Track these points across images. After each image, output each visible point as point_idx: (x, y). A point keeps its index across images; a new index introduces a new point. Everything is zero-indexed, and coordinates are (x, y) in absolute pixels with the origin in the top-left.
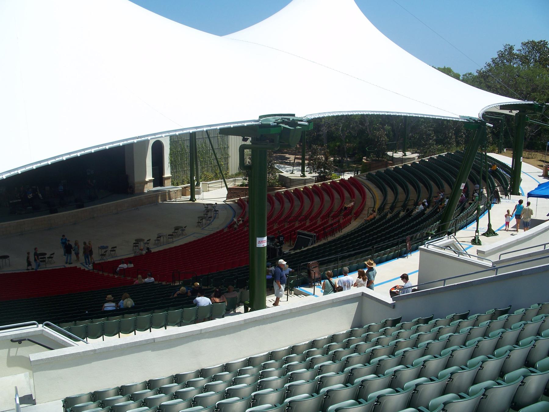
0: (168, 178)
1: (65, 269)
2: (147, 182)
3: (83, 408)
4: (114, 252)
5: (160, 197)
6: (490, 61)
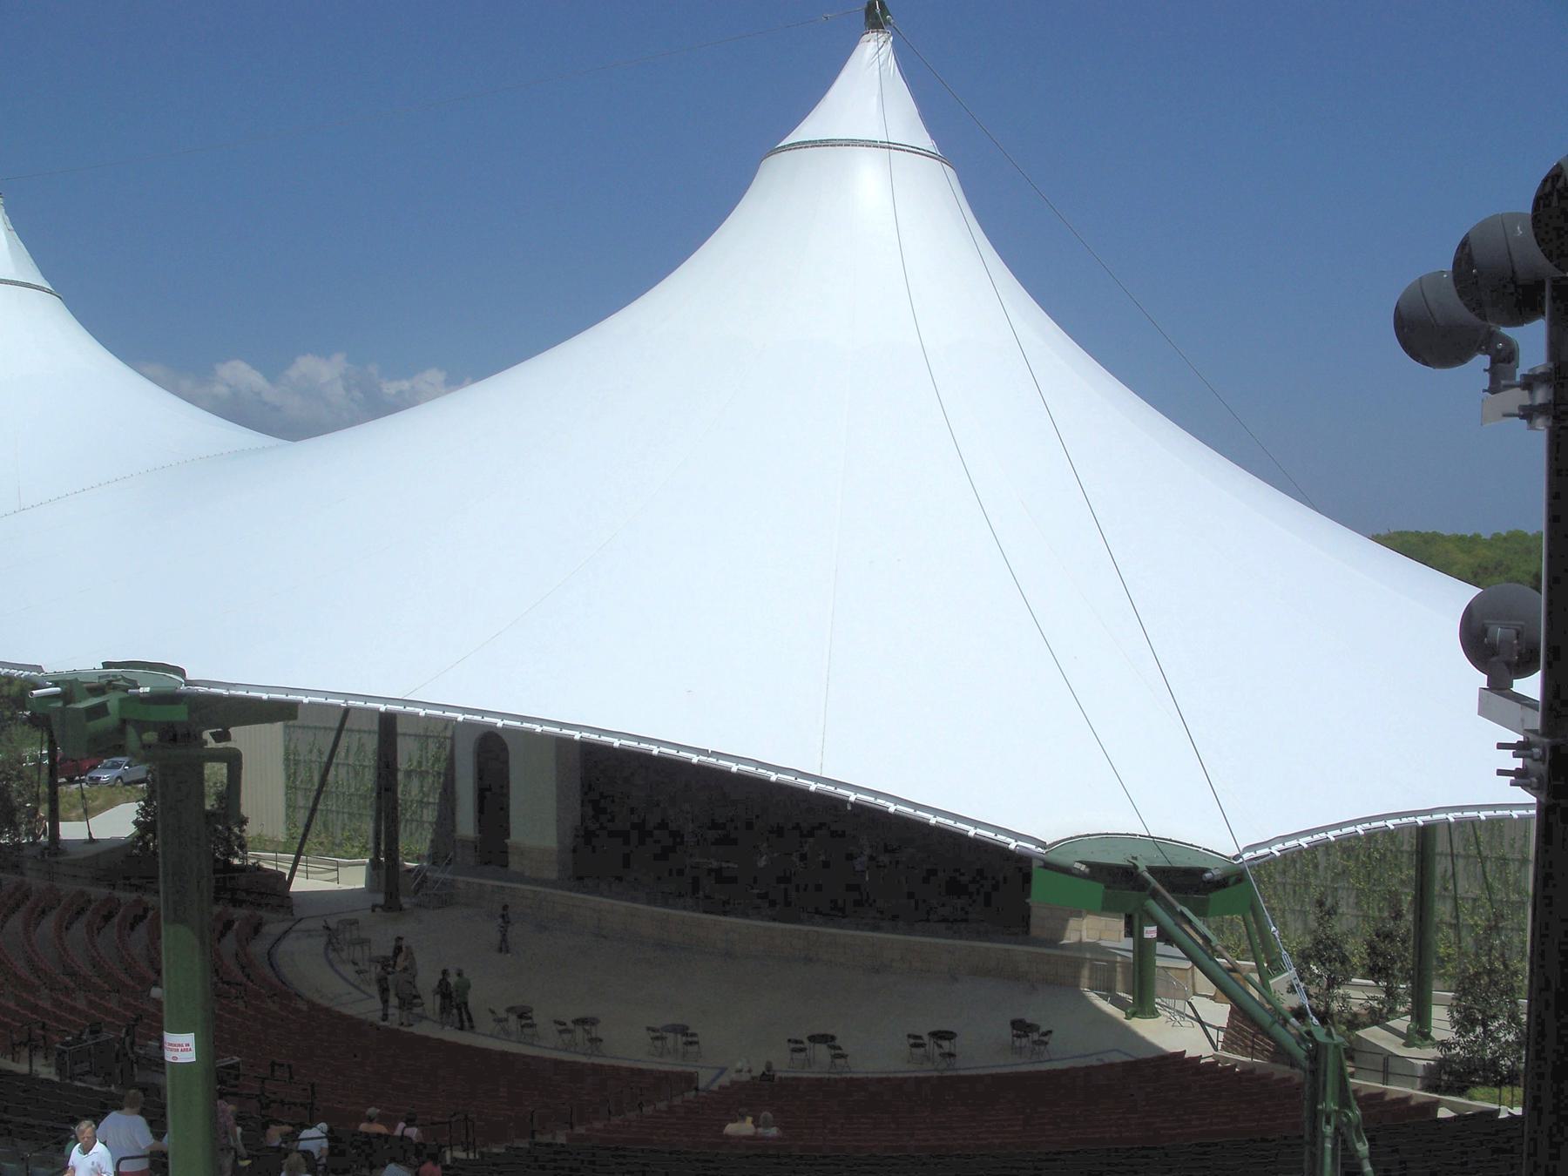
5: (1086, 972)
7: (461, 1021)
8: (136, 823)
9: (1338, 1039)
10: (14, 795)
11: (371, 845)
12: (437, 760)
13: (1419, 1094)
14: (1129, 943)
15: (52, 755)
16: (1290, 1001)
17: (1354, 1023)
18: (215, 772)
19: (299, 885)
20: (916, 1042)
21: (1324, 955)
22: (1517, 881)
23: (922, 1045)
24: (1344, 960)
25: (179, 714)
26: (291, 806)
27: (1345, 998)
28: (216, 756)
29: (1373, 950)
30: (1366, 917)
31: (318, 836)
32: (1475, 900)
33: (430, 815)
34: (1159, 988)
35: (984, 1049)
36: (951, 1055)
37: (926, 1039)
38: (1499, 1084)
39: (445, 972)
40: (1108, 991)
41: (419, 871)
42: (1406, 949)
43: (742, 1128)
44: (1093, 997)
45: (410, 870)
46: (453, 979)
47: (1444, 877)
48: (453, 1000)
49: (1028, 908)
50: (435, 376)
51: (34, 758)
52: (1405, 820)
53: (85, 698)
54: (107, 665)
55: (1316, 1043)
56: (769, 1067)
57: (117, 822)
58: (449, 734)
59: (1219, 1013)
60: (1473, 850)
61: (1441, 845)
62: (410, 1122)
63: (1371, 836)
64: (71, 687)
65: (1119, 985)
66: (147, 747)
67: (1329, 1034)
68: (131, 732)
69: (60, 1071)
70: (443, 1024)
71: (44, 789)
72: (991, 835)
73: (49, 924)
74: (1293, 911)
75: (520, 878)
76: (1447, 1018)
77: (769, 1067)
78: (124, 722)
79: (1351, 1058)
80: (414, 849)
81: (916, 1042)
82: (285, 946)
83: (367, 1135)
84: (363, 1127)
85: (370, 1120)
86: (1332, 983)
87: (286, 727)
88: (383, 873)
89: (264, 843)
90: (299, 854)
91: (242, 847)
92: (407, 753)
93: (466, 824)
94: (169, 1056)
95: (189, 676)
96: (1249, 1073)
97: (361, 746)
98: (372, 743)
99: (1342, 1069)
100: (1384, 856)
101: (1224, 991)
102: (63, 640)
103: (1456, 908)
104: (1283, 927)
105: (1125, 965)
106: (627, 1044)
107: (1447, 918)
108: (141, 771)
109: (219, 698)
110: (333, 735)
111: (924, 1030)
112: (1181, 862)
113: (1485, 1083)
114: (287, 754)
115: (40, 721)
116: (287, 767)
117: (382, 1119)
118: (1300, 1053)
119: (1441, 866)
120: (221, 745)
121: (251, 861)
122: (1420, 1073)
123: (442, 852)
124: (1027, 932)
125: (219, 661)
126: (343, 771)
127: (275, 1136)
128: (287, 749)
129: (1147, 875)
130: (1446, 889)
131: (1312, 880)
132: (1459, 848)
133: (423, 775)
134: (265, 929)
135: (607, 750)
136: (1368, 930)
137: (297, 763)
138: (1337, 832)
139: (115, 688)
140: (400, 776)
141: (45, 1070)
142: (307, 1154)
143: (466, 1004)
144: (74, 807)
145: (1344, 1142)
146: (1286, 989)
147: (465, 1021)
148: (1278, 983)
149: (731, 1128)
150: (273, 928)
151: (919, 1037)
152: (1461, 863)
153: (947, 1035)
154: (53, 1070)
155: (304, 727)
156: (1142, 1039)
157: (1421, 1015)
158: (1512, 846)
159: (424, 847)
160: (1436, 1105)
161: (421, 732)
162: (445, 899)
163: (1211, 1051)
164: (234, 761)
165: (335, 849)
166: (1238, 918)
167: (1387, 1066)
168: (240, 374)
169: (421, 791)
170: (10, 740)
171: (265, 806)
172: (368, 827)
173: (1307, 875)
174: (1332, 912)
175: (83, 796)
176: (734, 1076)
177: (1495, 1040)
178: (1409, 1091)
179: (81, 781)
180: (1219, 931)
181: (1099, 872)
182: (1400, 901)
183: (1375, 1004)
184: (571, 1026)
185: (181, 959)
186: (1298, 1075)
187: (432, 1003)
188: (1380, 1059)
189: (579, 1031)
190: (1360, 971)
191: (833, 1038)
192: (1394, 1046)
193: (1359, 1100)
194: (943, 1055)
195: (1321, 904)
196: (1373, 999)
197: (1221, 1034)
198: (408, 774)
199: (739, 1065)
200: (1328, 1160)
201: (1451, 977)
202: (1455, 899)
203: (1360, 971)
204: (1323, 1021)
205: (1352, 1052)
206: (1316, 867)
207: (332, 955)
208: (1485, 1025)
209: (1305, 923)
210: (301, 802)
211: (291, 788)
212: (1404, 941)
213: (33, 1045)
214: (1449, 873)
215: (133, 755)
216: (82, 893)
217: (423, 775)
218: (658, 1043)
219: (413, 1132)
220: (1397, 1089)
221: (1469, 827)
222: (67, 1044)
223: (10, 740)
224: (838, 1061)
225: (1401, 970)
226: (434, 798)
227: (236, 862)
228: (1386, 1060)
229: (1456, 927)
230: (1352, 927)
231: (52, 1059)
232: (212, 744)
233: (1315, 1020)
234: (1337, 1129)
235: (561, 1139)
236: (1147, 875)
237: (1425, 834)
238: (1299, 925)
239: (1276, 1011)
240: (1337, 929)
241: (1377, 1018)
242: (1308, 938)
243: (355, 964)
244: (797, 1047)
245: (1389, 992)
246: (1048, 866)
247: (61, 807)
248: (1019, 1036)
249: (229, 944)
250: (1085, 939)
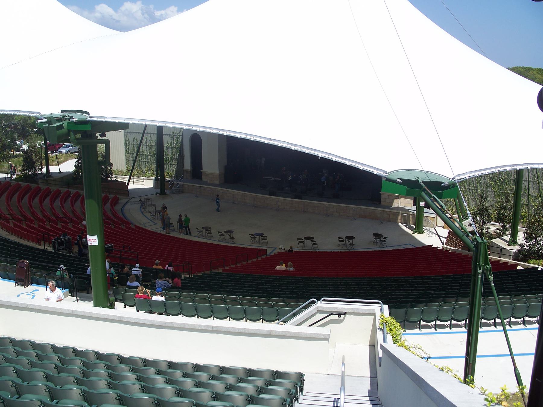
5: (400, 218)
7: (187, 232)
8: (75, 166)
9: (485, 241)
10: (34, 157)
11: (155, 173)
12: (177, 143)
13: (511, 261)
14: (415, 208)
15: (46, 143)
16: (470, 229)
17: (491, 237)
18: (101, 148)
19: (131, 186)
20: (341, 239)
21: (482, 214)
23: (343, 241)
24: (489, 216)
25: (88, 128)
26: (127, 160)
27: (488, 229)
28: (101, 142)
29: (499, 213)
30: (497, 202)
31: (137, 170)
32: (535, 197)
33: (175, 162)
34: (424, 224)
35: (364, 242)
36: (353, 244)
37: (344, 239)
38: (539, 259)
39: (180, 216)
40: (407, 225)
41: (171, 181)
42: (510, 213)
43: (282, 267)
44: (402, 226)
45: (169, 181)
46: (183, 218)
47: (525, 188)
48: (184, 225)
49: (380, 195)
50: (173, 9)
51: (39, 145)
52: (513, 168)
53: (56, 123)
54: (62, 111)
55: (478, 242)
56: (291, 247)
57: (69, 166)
58: (181, 134)
59: (445, 233)
60: (536, 180)
61: (525, 177)
62: (170, 266)
63: (500, 173)
64: (51, 120)
65: (411, 222)
66: (77, 139)
67: (482, 239)
68: (72, 133)
69: (54, 247)
70: (180, 233)
71: (43, 155)
72: (368, 169)
73: (47, 201)
74: (472, 199)
76: (523, 236)
77: (291, 247)
78: (69, 131)
79: (489, 249)
80: (170, 174)
81: (341, 239)
82: (127, 207)
83: (156, 269)
84: (154, 267)
85: (157, 264)
86: (484, 223)
87: (125, 132)
88: (159, 182)
89: (118, 172)
90: (130, 176)
91: (112, 174)
92: (167, 141)
93: (188, 165)
94: (89, 243)
95: (90, 115)
96: (454, 252)
97: (151, 139)
98: (154, 138)
99: (486, 252)
101: (448, 223)
102: (43, 101)
103: (529, 199)
104: (468, 203)
105: (413, 215)
106: (243, 239)
107: (525, 203)
108: (76, 148)
109: (101, 122)
110: (141, 135)
111: (344, 235)
112: (434, 179)
113: (534, 258)
114: (126, 142)
115: (41, 132)
116: (126, 146)
117: (160, 264)
118: (472, 246)
119: (524, 184)
120: (102, 138)
121: (114, 179)
122: (512, 254)
123: (179, 174)
124: (380, 203)
125: (100, 111)
126: (145, 147)
127: (126, 269)
128: (125, 140)
129: (422, 183)
130: (525, 193)
131: (479, 188)
132: (531, 178)
133: (172, 148)
134: (120, 201)
135: (235, 138)
136: (497, 205)
137: (129, 145)
138: (489, 171)
139: (66, 119)
140: (165, 149)
141: (49, 249)
142: (136, 275)
143: (188, 226)
144: (54, 161)
145: (485, 276)
146: (469, 225)
147: (188, 232)
148: (466, 223)
149: (278, 268)
150: (123, 201)
151: (342, 238)
152: (531, 184)
153: (352, 238)
154: (52, 248)
155: (131, 132)
156: (418, 241)
157: (514, 235)
159: (173, 173)
160: (517, 265)
161: (171, 133)
162: (181, 191)
163: (442, 245)
164: (107, 143)
165: (143, 174)
166: (452, 200)
167: (501, 252)
168: (104, 9)
169: (172, 154)
170: (31, 139)
171: (118, 159)
172: (154, 166)
173: (477, 186)
174: (486, 199)
175: (57, 157)
176: (279, 251)
177: (539, 244)
178: (508, 260)
179: (56, 152)
180: (446, 204)
181: (405, 182)
182: (509, 196)
183: (498, 231)
184: (224, 233)
185: (92, 212)
186: (471, 254)
187: (176, 225)
188: (499, 249)
189: (227, 235)
190: (494, 220)
192: (504, 245)
193: (491, 263)
194: (350, 244)
195: (481, 196)
196: (498, 229)
197: (445, 240)
198: (167, 148)
199: (280, 247)
200: (479, 281)
201: (525, 222)
202: (528, 196)
203: (494, 220)
204: (480, 236)
205: (491, 246)
206: (481, 184)
207: (143, 210)
208: (536, 239)
209: (476, 203)
210: (131, 159)
211: (127, 153)
212: (509, 210)
213: (46, 240)
214: (527, 187)
215: (73, 142)
216: (58, 190)
217: (172, 148)
218: (253, 239)
219: (171, 268)
220: (504, 260)
221: (535, 171)
222: (56, 240)
223: (31, 139)
224: (314, 246)
225: (508, 220)
226: (176, 156)
227: (109, 179)
228: (501, 250)
229: (528, 206)
230: (492, 204)
231: (51, 245)
232: (99, 138)
233: (478, 235)
234: (483, 271)
235: (221, 271)
236: (422, 183)
237: (519, 173)
238: (474, 203)
239: (465, 231)
240: (487, 205)
241: (499, 235)
242: (476, 208)
243: (151, 213)
244: (300, 241)
245: (504, 227)
246: (388, 180)
247: (50, 161)
248: (376, 239)
249: (108, 206)
250: (400, 206)
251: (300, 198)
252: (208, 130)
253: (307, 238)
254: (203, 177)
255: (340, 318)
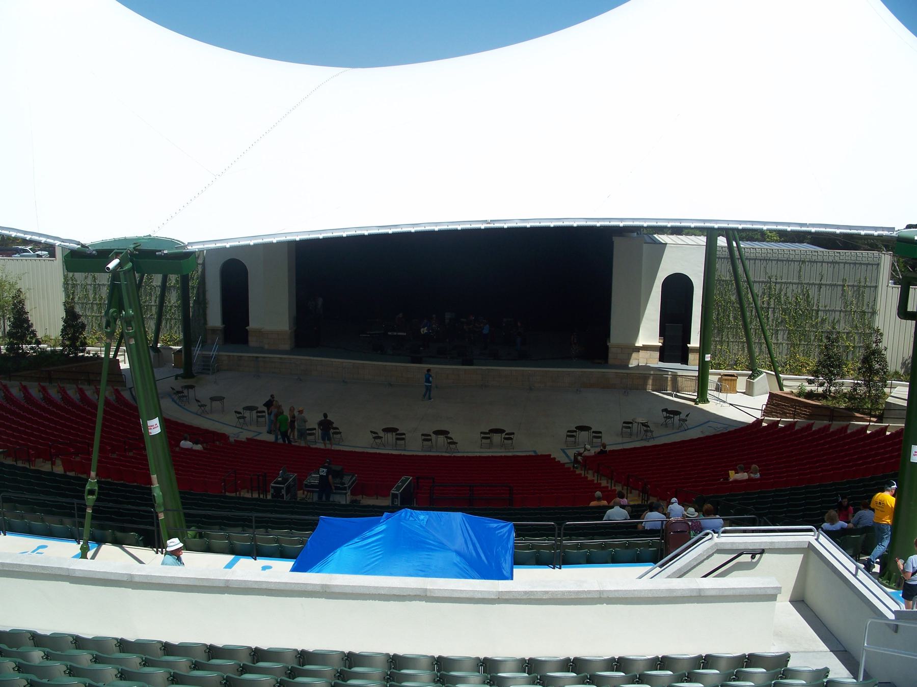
0: (694, 350)
1: (88, 272)
2: (638, 349)
3: (408, 678)
4: (510, 441)
5: (650, 382)
6: (34, 328)
22: (869, 323)
58: (200, 261)
75: (261, 350)
84: (593, 504)
85: (599, 499)
93: (215, 318)
100: (803, 312)
116: (66, 290)
137: (74, 286)
158: (868, 305)
191: (447, 432)
206: (768, 319)
251: (471, 363)
252: (219, 245)
253: (438, 433)
254: (250, 338)
255: (754, 560)
